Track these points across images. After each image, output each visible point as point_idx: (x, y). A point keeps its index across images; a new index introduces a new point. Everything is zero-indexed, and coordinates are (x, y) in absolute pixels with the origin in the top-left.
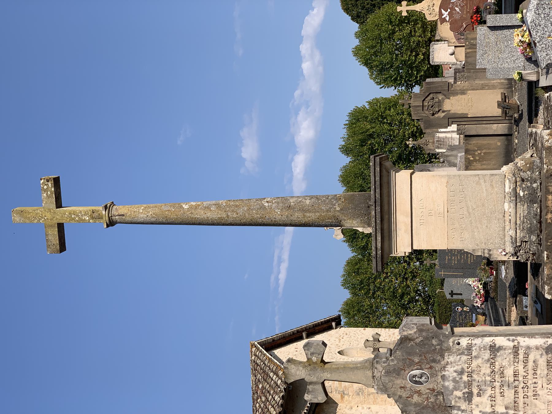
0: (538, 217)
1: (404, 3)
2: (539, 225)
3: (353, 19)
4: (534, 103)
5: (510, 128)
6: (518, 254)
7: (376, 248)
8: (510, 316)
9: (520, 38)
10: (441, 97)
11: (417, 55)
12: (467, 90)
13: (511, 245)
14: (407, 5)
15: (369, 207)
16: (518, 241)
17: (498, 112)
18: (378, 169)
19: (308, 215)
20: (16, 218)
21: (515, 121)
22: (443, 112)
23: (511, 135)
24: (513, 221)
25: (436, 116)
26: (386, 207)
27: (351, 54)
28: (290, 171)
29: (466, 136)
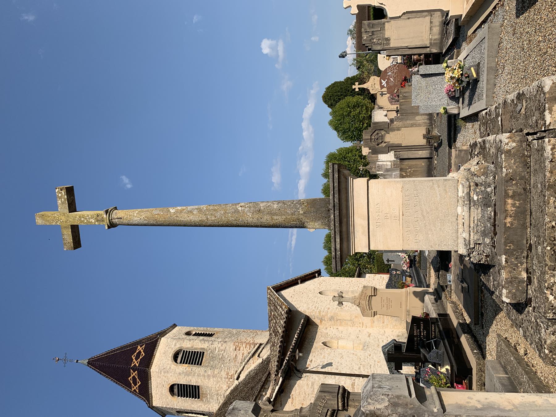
0: (492, 221)
1: (357, 83)
2: (493, 229)
3: (329, 106)
4: (453, 133)
5: (431, 154)
6: (471, 255)
7: (335, 249)
8: (430, 280)
9: (451, 74)
10: (383, 132)
11: (363, 124)
12: (401, 127)
13: (464, 247)
14: (359, 84)
15: (329, 211)
16: (472, 243)
17: (423, 142)
18: (336, 176)
19: (275, 217)
20: (39, 221)
21: (435, 148)
22: (385, 143)
23: (432, 158)
24: (466, 224)
25: (380, 145)
26: (344, 211)
27: (328, 124)
28: (297, 188)
29: (400, 159)
